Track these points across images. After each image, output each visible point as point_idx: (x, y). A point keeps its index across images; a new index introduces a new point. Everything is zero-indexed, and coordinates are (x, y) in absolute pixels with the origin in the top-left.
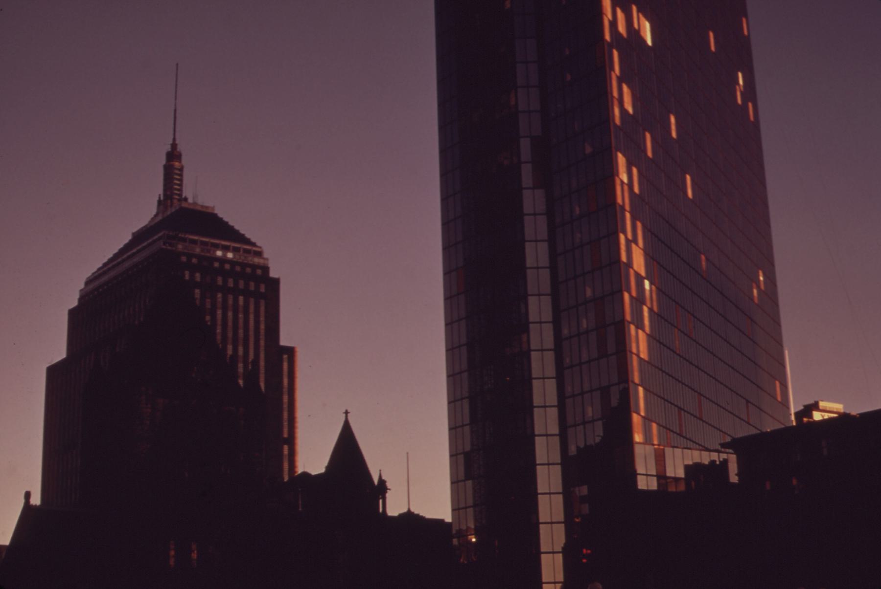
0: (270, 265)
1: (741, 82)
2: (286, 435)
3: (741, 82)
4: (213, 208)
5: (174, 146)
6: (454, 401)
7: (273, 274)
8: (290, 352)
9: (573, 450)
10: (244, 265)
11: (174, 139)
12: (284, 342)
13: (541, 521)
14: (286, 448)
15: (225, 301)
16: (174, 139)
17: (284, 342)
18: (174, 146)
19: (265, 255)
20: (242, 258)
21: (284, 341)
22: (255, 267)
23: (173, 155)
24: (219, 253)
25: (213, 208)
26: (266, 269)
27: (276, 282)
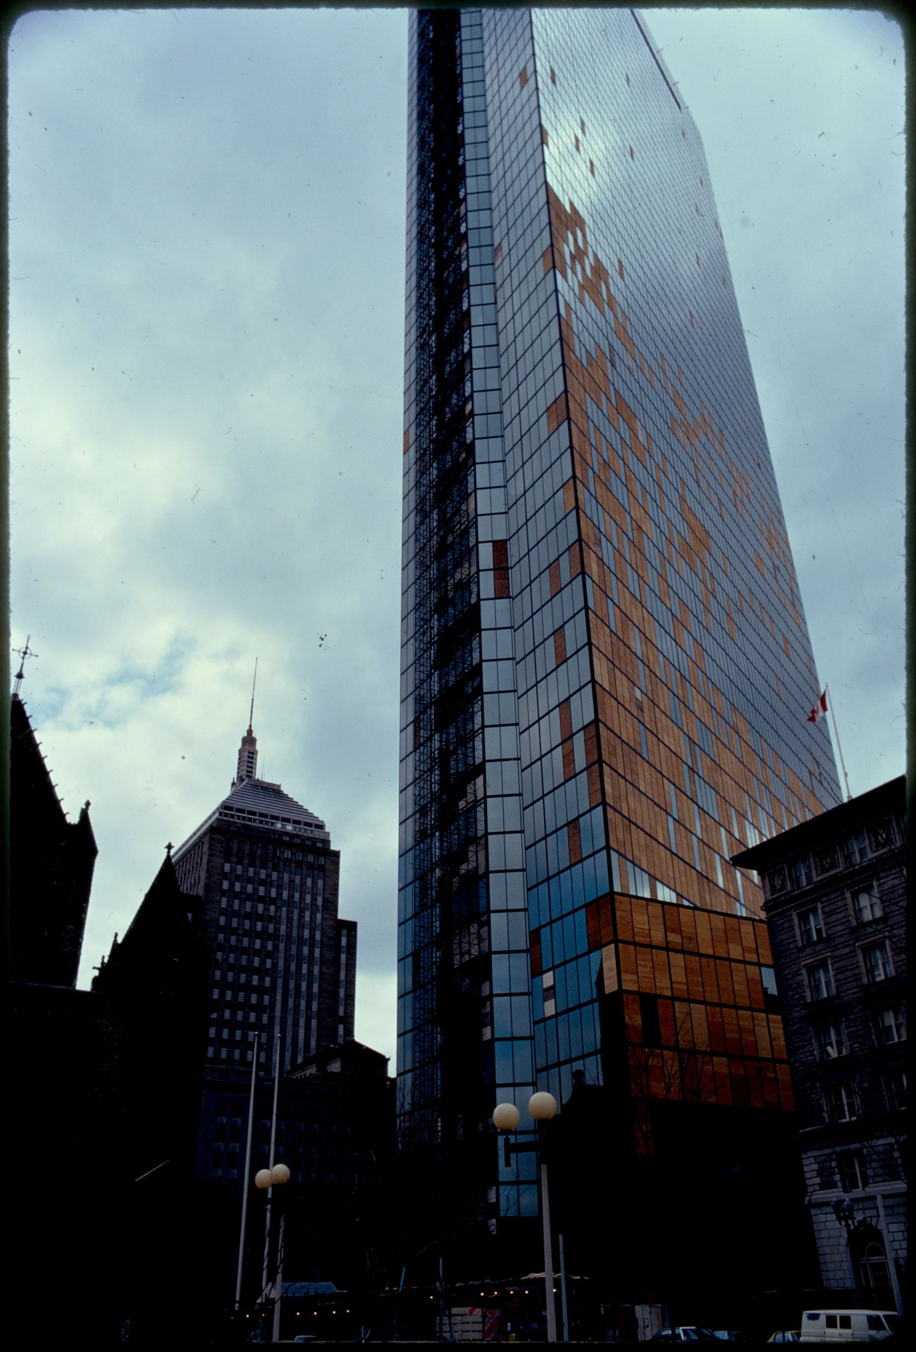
0: (331, 838)
1: (905, 1083)
2: (341, 1013)
3: (905, 1083)
4: (279, 786)
5: (250, 732)
6: (404, 887)
7: (333, 847)
8: (351, 927)
9: (482, 777)
10: (304, 839)
11: (250, 726)
12: (342, 915)
13: (498, 1081)
14: (341, 1028)
15: (303, 883)
16: (250, 726)
17: (342, 915)
18: (250, 732)
19: (327, 830)
20: (303, 831)
21: (344, 913)
22: (314, 840)
23: (249, 741)
24: (279, 826)
25: (279, 786)
26: (327, 842)
27: (337, 854)
